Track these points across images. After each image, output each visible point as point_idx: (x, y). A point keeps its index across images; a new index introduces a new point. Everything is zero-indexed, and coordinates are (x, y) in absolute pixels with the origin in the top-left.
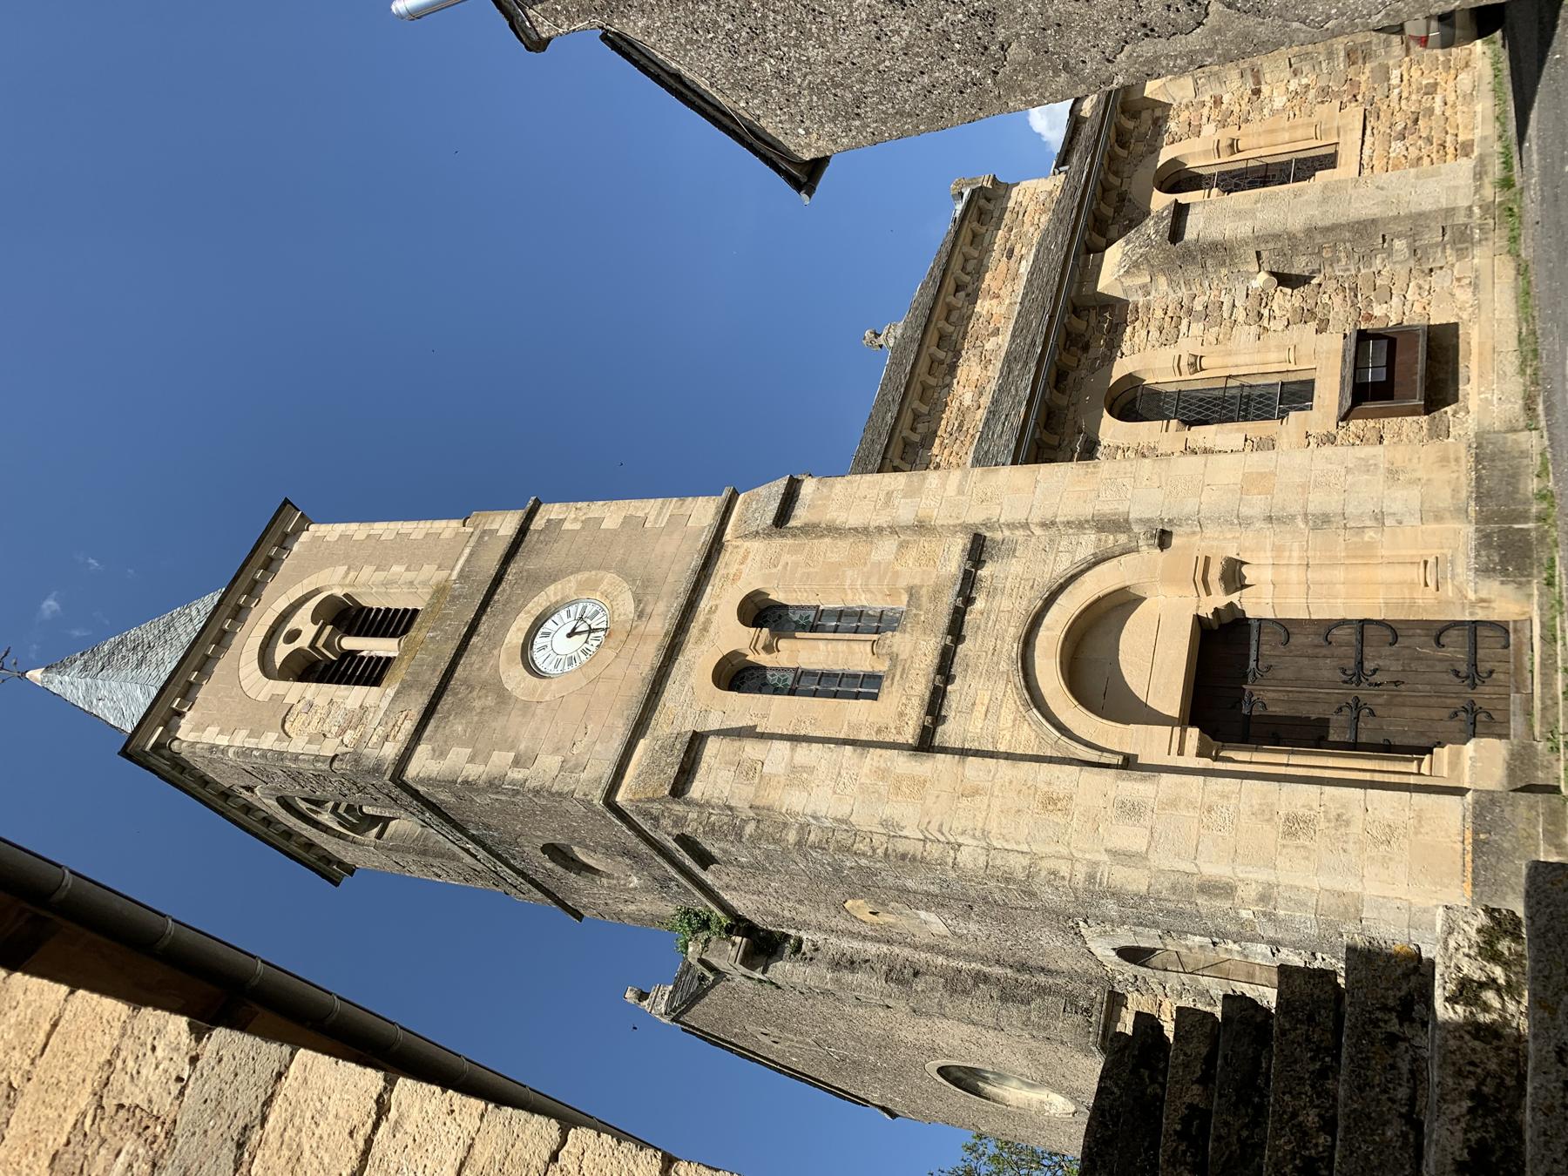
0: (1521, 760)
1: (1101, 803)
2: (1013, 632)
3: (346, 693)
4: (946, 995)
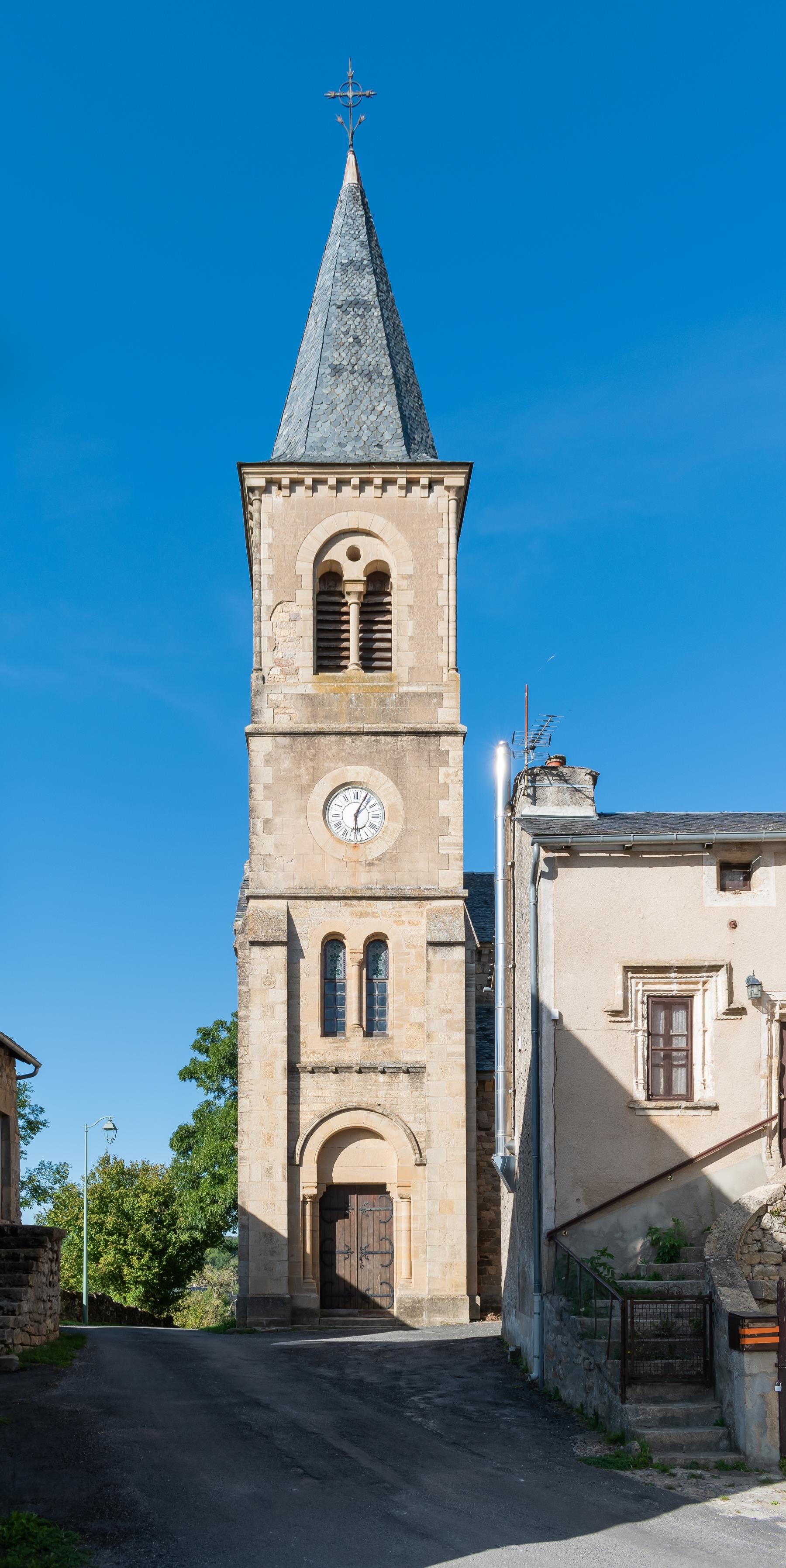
0: (308, 1313)
2: (363, 1100)
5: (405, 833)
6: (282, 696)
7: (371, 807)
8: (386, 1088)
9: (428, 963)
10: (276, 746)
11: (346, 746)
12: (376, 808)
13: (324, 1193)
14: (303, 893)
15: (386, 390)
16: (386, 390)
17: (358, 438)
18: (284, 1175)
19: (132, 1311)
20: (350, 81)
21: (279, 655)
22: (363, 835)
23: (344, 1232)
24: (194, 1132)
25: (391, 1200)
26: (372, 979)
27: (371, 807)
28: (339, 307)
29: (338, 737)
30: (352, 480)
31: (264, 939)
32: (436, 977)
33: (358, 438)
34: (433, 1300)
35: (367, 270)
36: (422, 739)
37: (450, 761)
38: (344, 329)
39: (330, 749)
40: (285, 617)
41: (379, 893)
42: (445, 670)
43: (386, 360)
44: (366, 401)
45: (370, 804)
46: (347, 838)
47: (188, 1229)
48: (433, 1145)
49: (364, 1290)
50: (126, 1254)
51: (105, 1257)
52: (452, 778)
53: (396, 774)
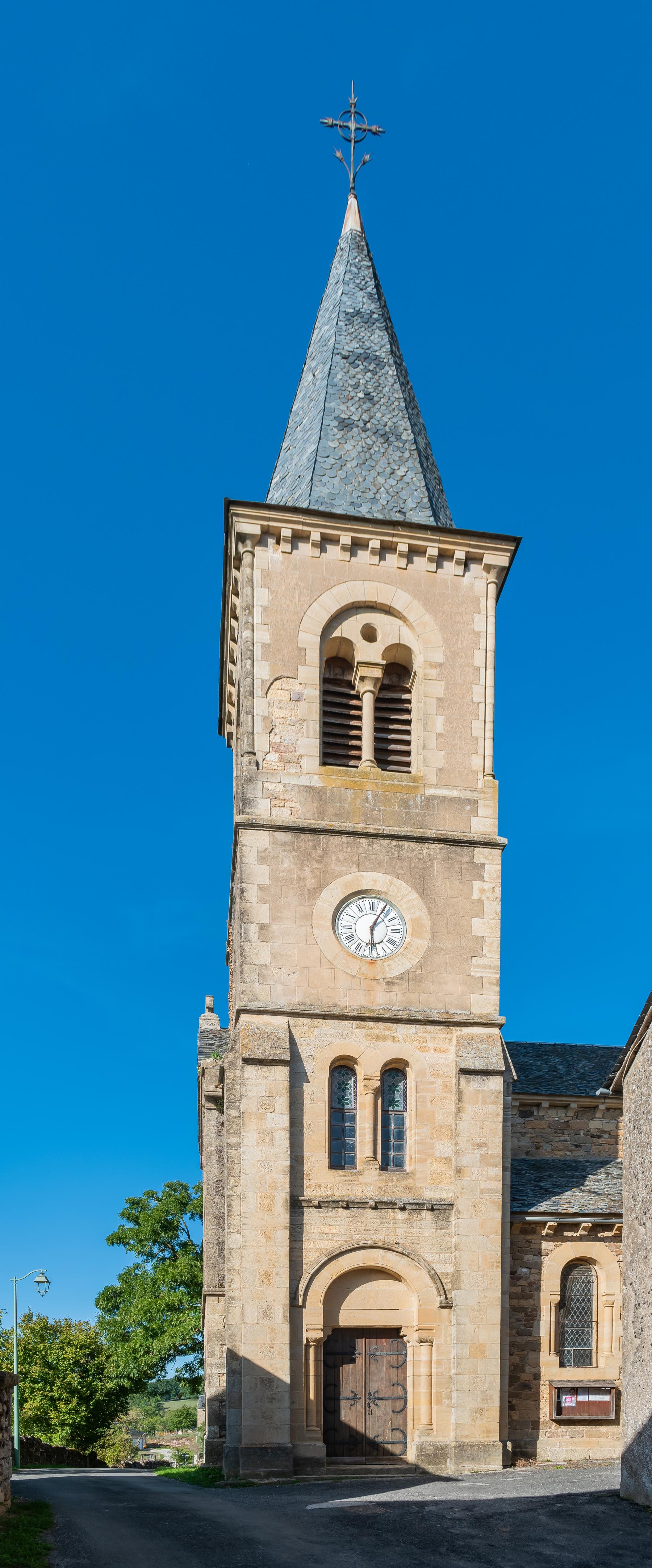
0: (314, 1463)
2: (380, 1238)
3: (311, 733)
4: (215, 1215)
5: (431, 951)
6: (281, 786)
7: (390, 921)
8: (406, 1226)
9: (460, 1092)
10: (274, 842)
11: (361, 849)
12: (396, 921)
13: (329, 1336)
14: (308, 1010)
15: (407, 454)
16: (407, 454)
17: (374, 500)
18: (285, 1317)
19: (60, 1450)
20: (353, 110)
21: (277, 739)
22: (380, 950)
23: (350, 1377)
24: (121, 1293)
25: (404, 1345)
26: (388, 1111)
27: (390, 921)
28: (345, 358)
29: (351, 839)
30: (371, 542)
31: (261, 1057)
32: (469, 1109)
33: (374, 500)
35: (378, 324)
36: (453, 848)
37: (486, 876)
38: (353, 383)
39: (342, 851)
40: (285, 696)
41: (401, 1015)
42: (480, 776)
43: (405, 424)
44: (382, 463)
45: (390, 917)
46: (361, 953)
47: (117, 1377)
48: (463, 1286)
50: (52, 1400)
51: (31, 1402)
52: (488, 894)
53: (422, 883)
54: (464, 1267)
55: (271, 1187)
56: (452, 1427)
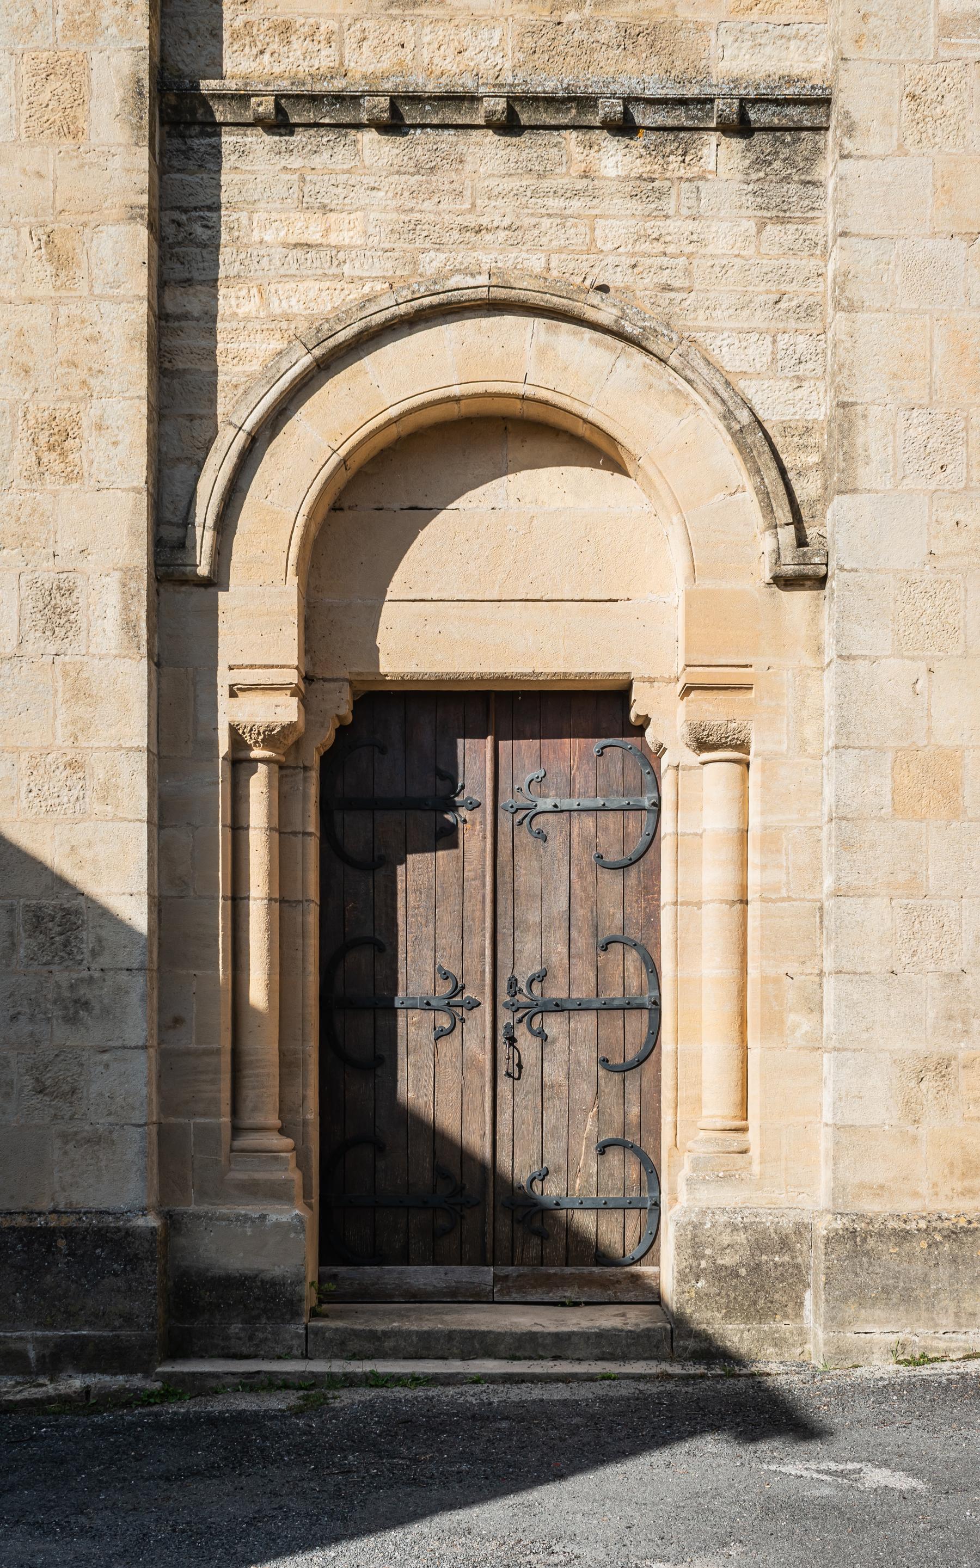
0: (260, 1300)
1: (67, 544)
2: (524, 267)
8: (633, 205)
18: (128, 626)
23: (435, 907)
25: (649, 762)
34: (854, 1241)
48: (865, 476)
49: (522, 1177)
54: (868, 390)
55: (73, 26)
56: (824, 1142)
